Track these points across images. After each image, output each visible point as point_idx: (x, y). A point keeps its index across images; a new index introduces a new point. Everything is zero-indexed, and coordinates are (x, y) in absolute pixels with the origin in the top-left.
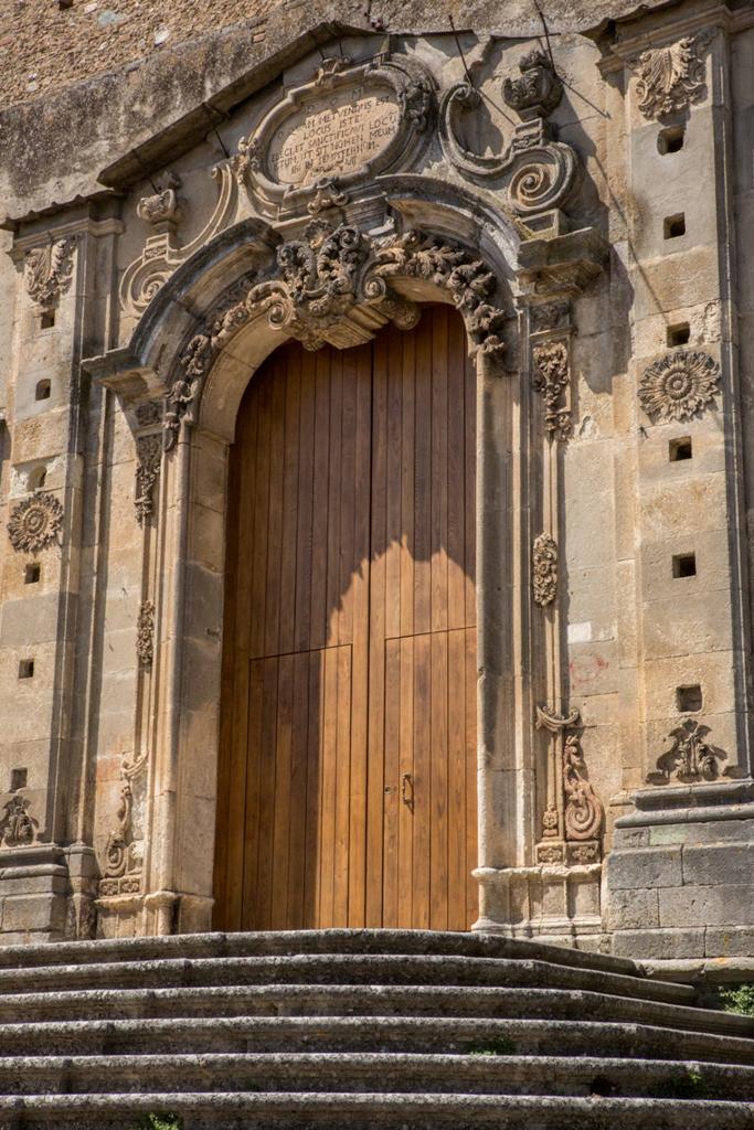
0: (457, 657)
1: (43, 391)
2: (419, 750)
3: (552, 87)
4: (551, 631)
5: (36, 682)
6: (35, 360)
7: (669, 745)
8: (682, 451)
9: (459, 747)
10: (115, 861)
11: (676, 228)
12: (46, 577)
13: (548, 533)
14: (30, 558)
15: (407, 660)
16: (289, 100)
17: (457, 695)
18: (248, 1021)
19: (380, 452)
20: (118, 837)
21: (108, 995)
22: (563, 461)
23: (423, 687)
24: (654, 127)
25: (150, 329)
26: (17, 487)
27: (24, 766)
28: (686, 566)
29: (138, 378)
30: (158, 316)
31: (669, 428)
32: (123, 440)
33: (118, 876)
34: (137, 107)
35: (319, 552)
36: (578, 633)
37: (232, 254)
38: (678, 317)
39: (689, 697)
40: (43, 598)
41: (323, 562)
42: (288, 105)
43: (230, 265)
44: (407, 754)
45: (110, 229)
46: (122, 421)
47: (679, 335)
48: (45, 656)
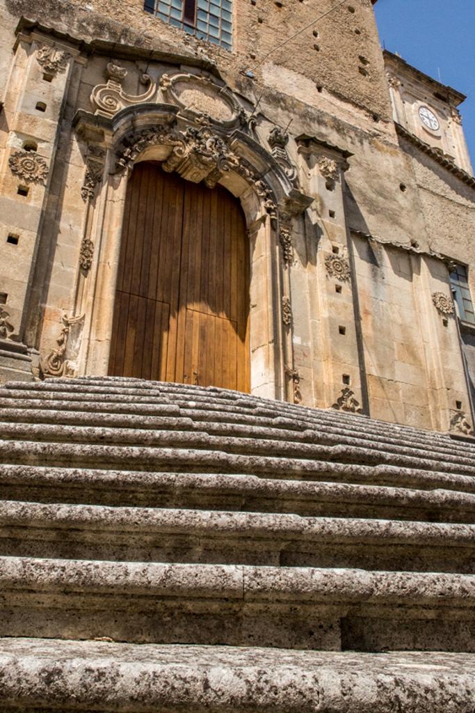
0: (219, 329)
1: (41, 107)
2: (201, 363)
3: (58, 148)
4: (288, 337)
5: (20, 249)
6: (37, 91)
7: (341, 394)
8: (338, 290)
9: (220, 368)
10: (56, 366)
11: (332, 214)
12: (33, 197)
13: (286, 297)
14: (23, 182)
15: (196, 322)
16: (188, 75)
17: (219, 345)
18: (75, 473)
19: (186, 228)
20: (60, 354)
21: (351, 468)
22: (49, 269)
23: (203, 336)
24: (324, 182)
25: (121, 118)
26: (14, 142)
27: (6, 292)
28: (342, 331)
29: (102, 134)
30: (125, 115)
31: (334, 280)
32: (76, 155)
33: (56, 375)
34: (84, 24)
35: (154, 257)
36: (297, 340)
37: (160, 114)
38: (337, 245)
39: (346, 379)
40: (31, 207)
41: (156, 261)
42: (187, 78)
43: (156, 117)
44: (195, 362)
45: (83, 63)
46: (76, 146)
47: (335, 250)
48: (29, 238)
